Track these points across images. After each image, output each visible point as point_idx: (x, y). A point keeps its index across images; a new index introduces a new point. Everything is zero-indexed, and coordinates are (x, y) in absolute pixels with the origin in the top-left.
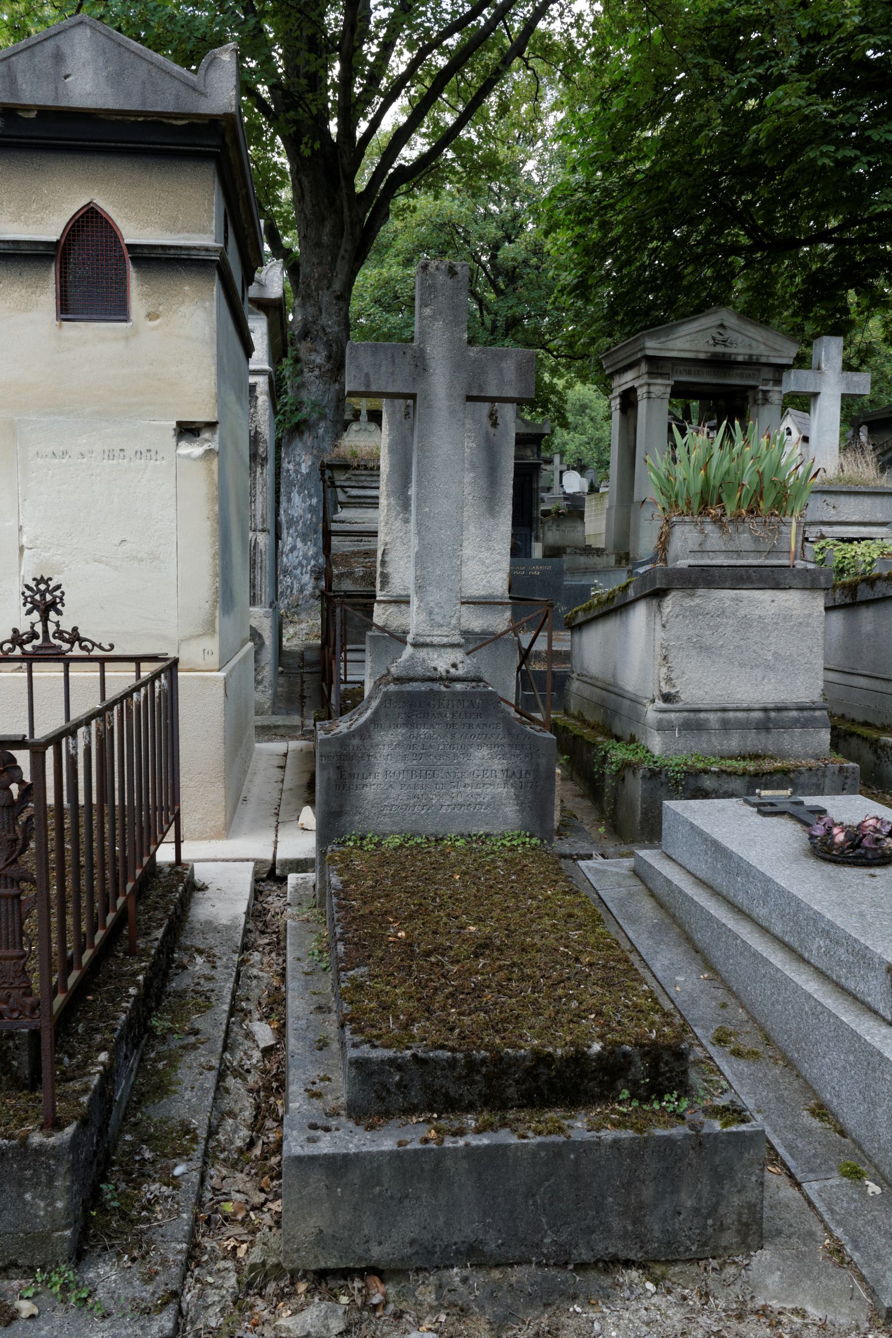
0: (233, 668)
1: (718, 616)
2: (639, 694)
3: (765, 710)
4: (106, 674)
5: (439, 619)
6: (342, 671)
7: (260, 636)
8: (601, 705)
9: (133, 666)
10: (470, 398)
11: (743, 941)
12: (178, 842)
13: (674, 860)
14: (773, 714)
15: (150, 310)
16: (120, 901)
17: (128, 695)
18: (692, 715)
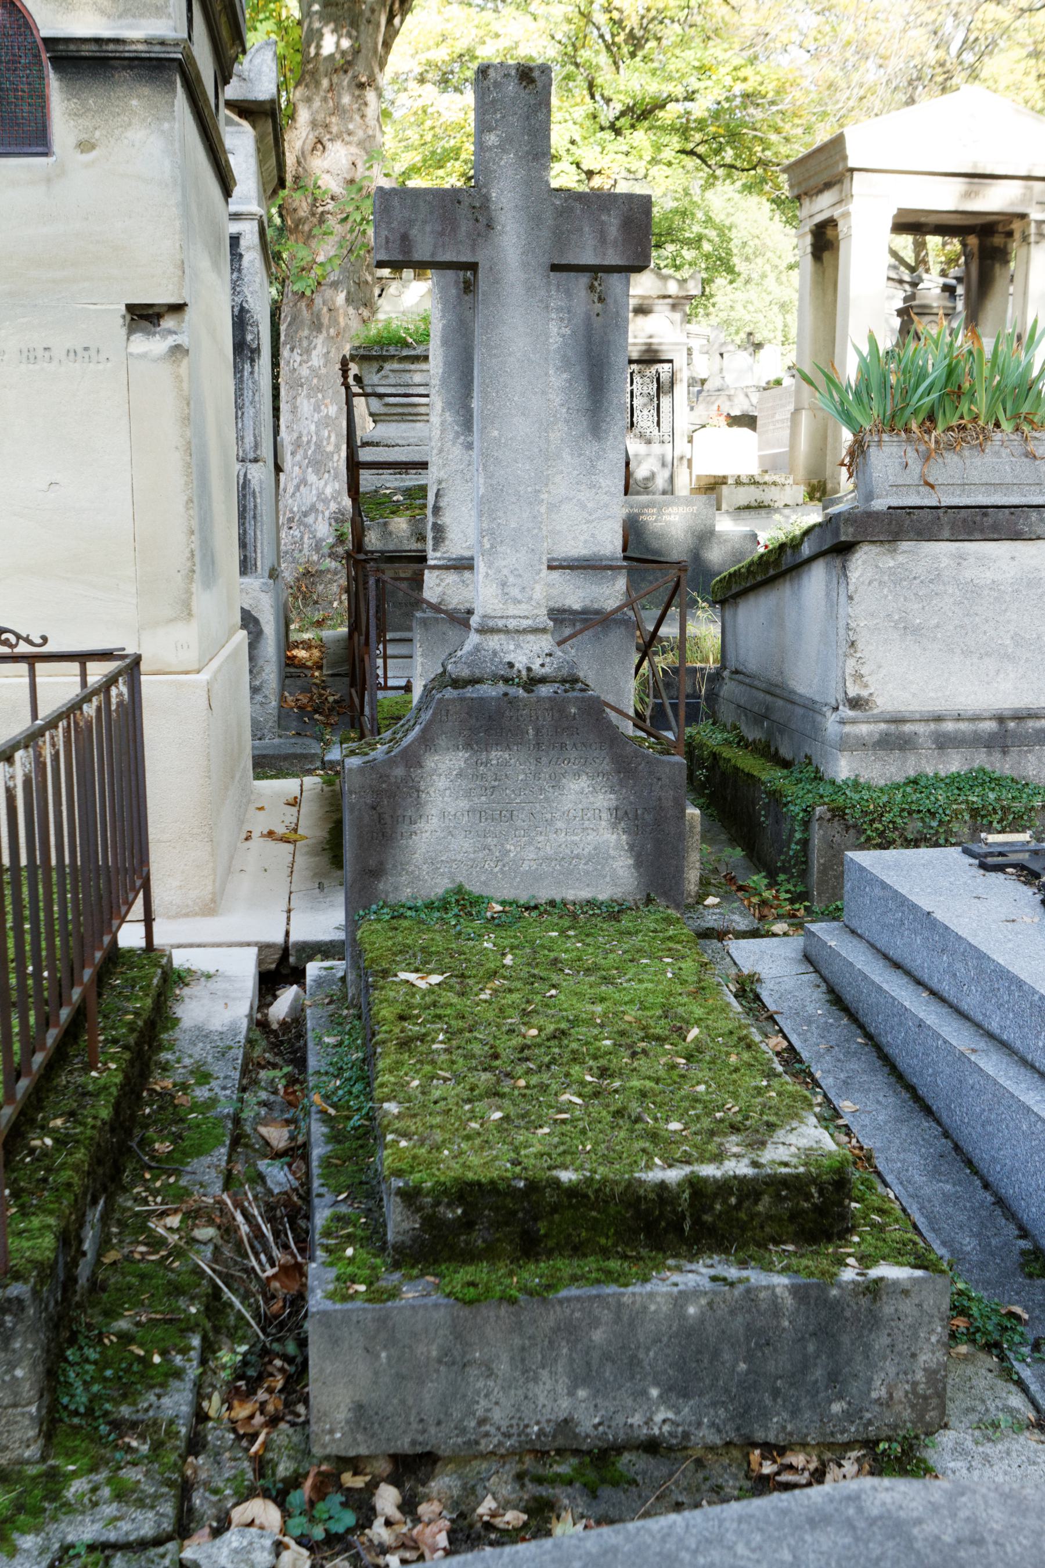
0: (220, 669)
1: (931, 581)
2: (817, 698)
3: (1001, 719)
4: (38, 680)
5: (515, 592)
6: (380, 672)
7: (256, 621)
8: (759, 717)
9: (75, 666)
10: (555, 268)
11: (945, 1042)
12: (148, 920)
13: (860, 936)
14: (1012, 725)
15: (83, 136)
16: (76, 994)
17: (76, 706)
18: (893, 727)
